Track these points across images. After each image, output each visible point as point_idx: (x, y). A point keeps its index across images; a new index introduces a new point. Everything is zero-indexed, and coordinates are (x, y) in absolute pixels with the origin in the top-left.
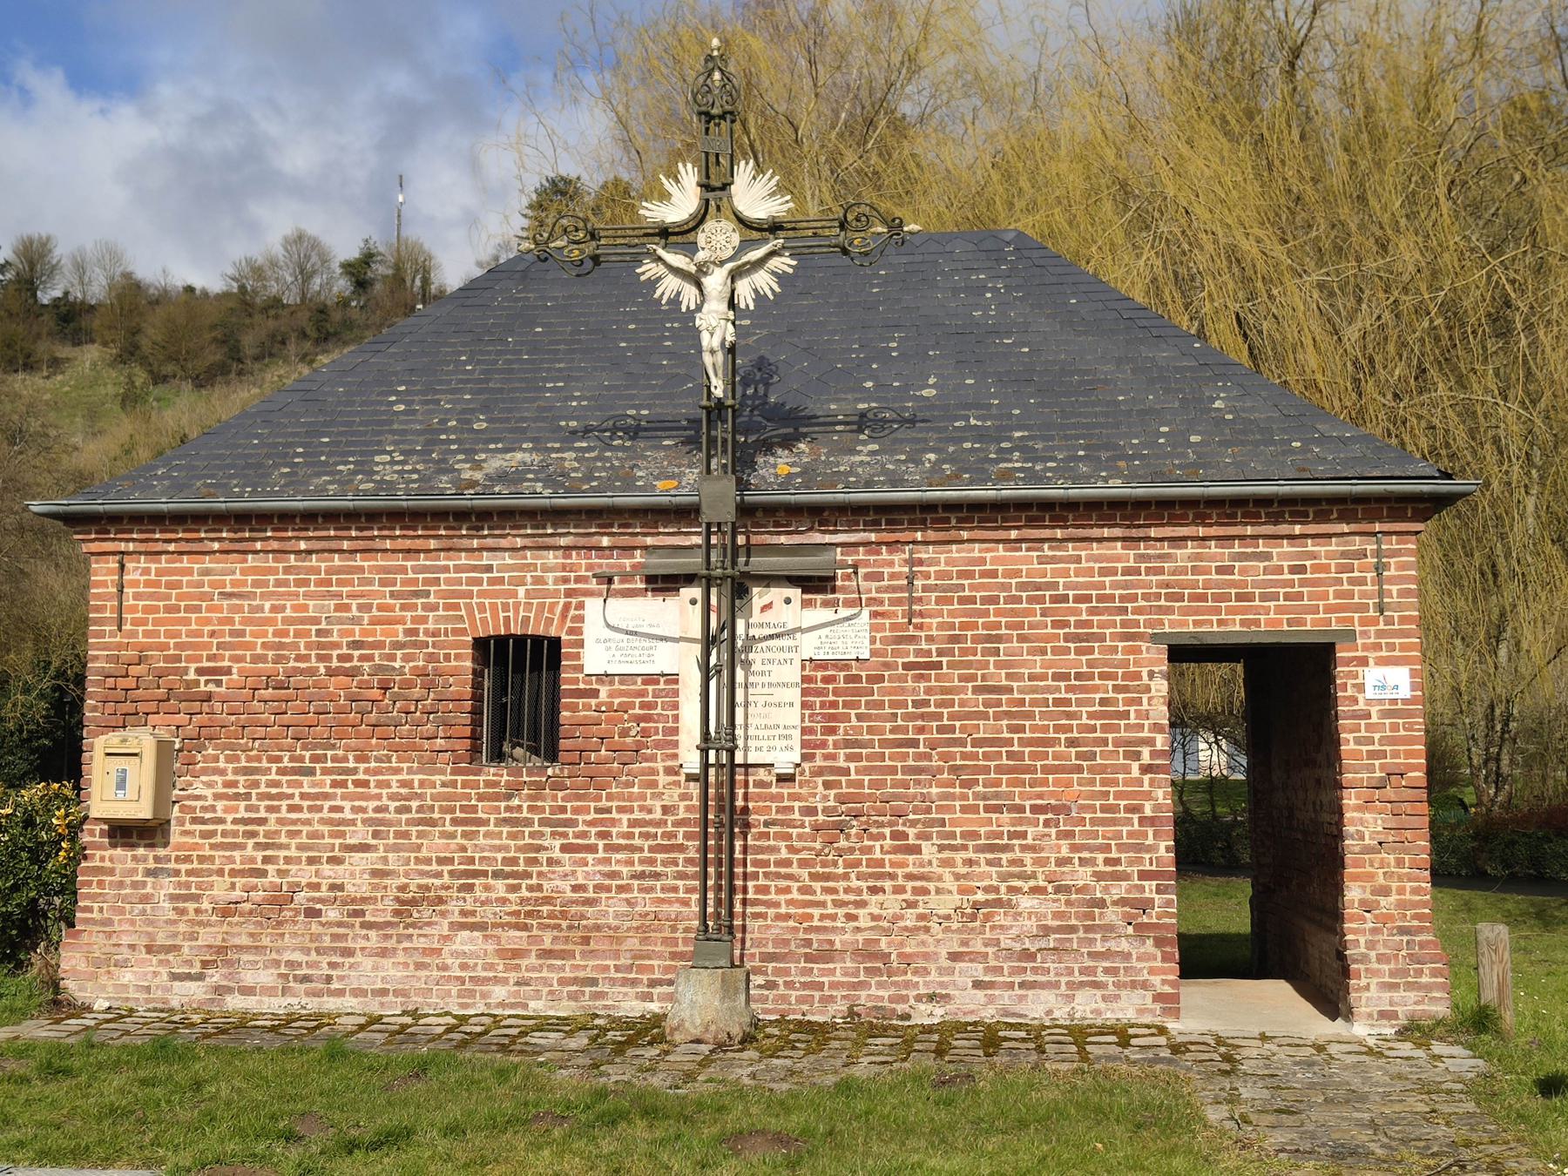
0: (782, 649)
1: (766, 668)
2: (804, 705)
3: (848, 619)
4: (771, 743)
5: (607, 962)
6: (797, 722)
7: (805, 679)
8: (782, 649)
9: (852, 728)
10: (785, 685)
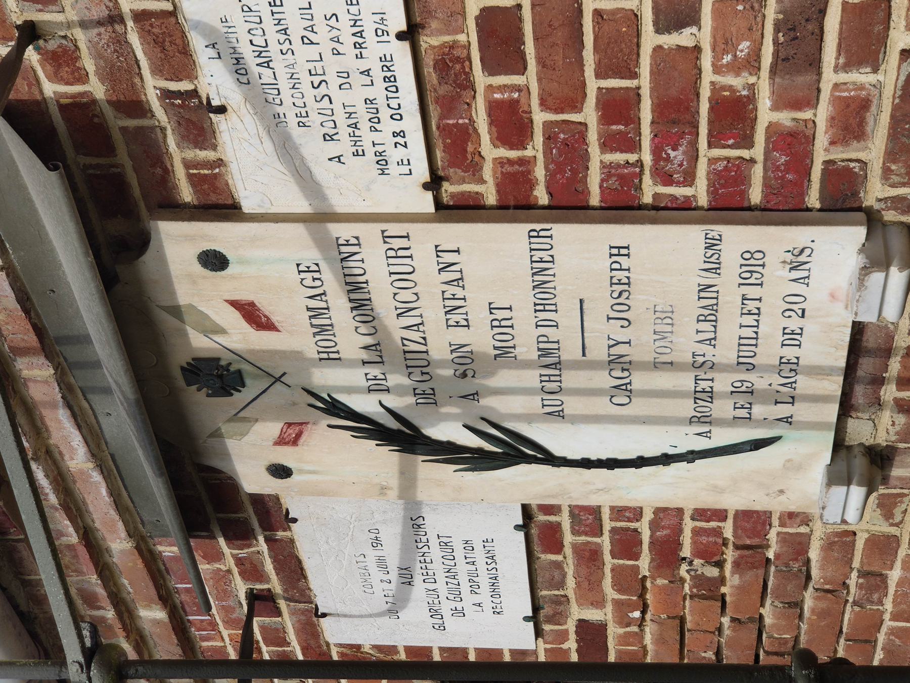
0: (402, 278)
1: (479, 316)
2: (623, 206)
3: (239, 68)
4: (772, 306)
5: (571, 582)
6: (690, 237)
7: (515, 205)
8: (402, 278)
9: (723, 43)
10: (541, 273)
